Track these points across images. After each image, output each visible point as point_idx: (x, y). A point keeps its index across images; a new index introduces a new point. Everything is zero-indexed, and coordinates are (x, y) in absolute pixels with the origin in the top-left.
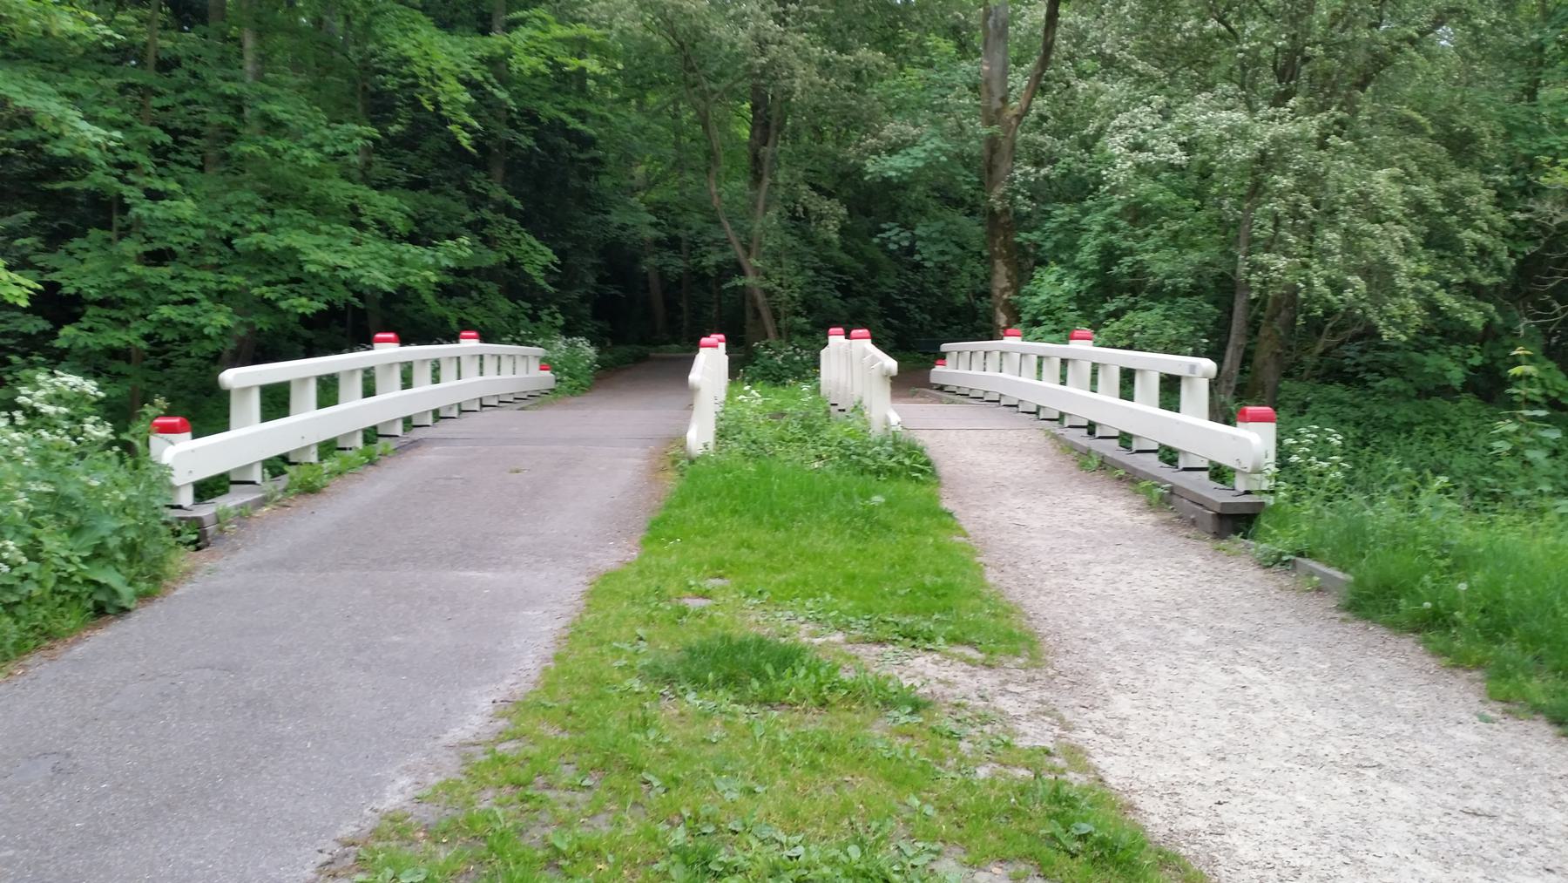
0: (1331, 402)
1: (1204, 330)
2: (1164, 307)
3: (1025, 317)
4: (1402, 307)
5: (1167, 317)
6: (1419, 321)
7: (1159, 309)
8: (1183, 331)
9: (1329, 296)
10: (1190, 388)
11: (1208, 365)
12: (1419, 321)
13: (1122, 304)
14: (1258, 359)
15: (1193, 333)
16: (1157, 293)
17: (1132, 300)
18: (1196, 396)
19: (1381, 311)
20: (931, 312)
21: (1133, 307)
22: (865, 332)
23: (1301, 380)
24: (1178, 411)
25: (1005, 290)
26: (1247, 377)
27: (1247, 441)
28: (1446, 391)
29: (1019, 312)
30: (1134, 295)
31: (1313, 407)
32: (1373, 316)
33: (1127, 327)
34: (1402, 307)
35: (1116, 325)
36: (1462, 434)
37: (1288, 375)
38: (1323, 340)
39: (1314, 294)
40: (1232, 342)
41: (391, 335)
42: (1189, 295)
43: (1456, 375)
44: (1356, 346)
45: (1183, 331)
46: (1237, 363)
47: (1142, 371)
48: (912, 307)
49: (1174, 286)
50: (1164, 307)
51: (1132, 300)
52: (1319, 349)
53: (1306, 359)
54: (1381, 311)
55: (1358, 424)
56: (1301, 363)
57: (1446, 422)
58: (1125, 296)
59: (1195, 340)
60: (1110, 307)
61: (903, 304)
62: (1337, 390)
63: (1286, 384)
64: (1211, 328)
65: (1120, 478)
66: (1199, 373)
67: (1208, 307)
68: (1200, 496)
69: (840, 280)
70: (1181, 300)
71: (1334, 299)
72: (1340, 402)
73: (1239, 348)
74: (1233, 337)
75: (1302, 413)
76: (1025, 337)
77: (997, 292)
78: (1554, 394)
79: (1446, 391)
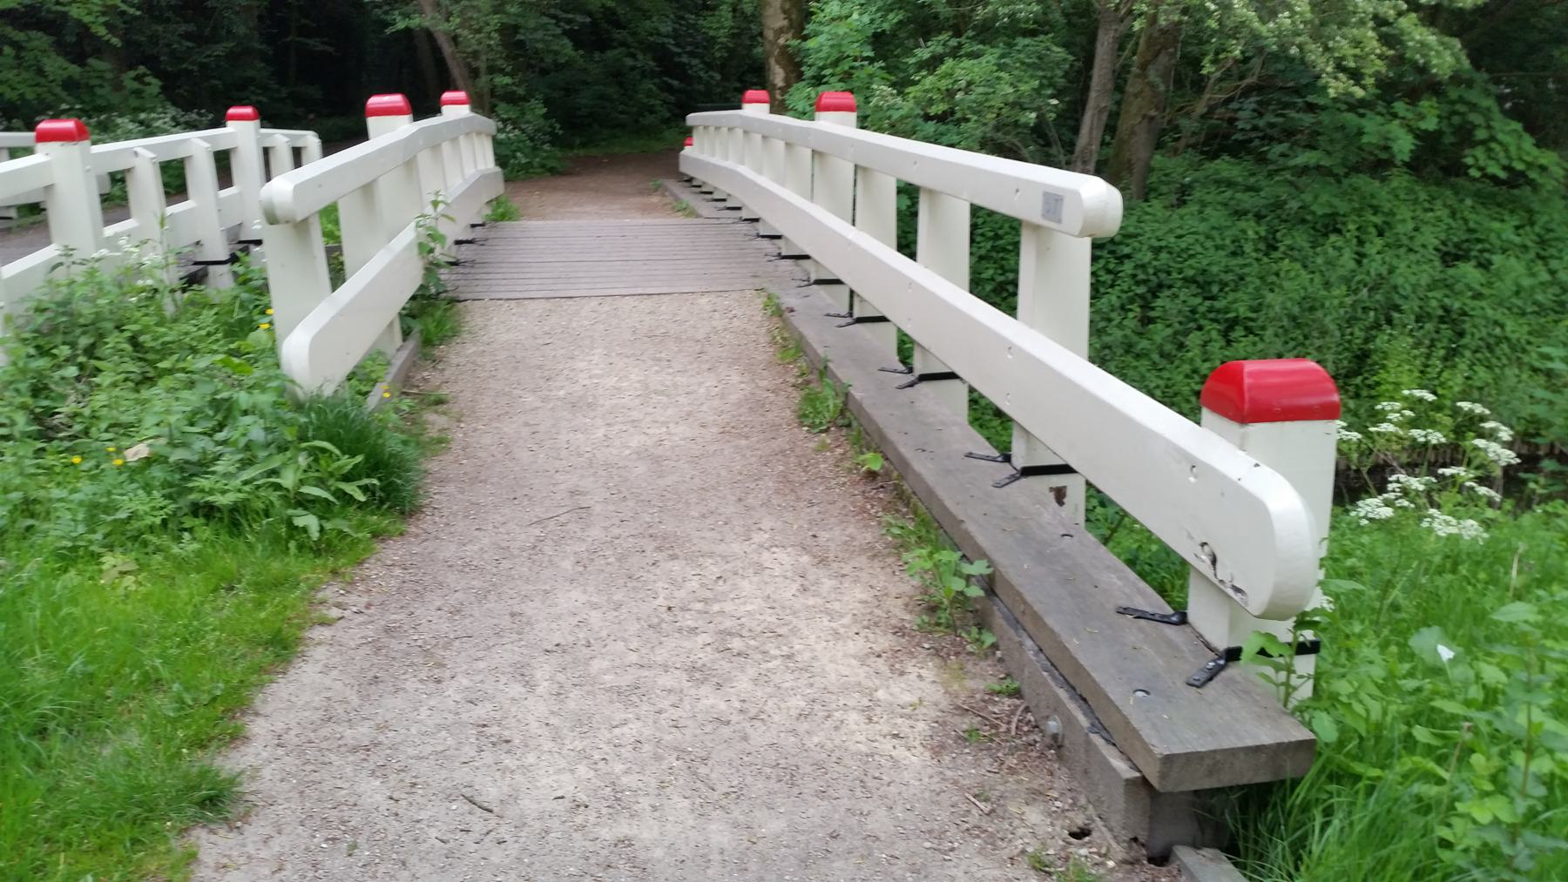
0: (1218, 182)
1: (1051, 85)
2: (997, 52)
3: (809, 73)
4: (1357, 43)
5: (1001, 67)
6: (1380, 66)
7: (991, 56)
8: (1023, 87)
9: (1256, 25)
10: (1042, 254)
11: (1095, 197)
12: (1380, 66)
13: (940, 50)
14: (1124, 125)
15: (1037, 91)
16: (987, 32)
17: (954, 42)
18: (1059, 277)
19: (1327, 49)
20: (722, 68)
21: (955, 53)
22: (396, 99)
23: (1176, 152)
24: (1011, 310)
25: (780, 31)
26: (1110, 151)
27: (1256, 508)
28: (1379, 165)
29: (800, 64)
30: (958, 34)
31: (1197, 194)
32: (1315, 54)
33: (944, 84)
34: (1357, 43)
35: (929, 81)
36: (1400, 229)
37: (1159, 146)
38: (1206, 96)
39: (1230, 23)
40: (1091, 103)
41: (248, 110)
42: (1032, 33)
43: (1404, 145)
44: (1251, 103)
45: (1023, 87)
46: (1098, 134)
47: (931, 192)
48: (695, 62)
49: (1012, 16)
50: (997, 52)
51: (954, 42)
52: (1201, 108)
53: (1184, 123)
54: (1327, 49)
55: (1259, 217)
56: (1176, 129)
57: (1376, 210)
58: (943, 37)
59: (1039, 102)
60: (923, 53)
61: (685, 59)
62: (1225, 167)
63: (1158, 159)
64: (1061, 82)
65: (872, 475)
66: (1072, 219)
67: (1059, 52)
68: (1079, 668)
69: (569, 21)
70: (1022, 42)
71: (1263, 30)
72: (1230, 184)
73: (1101, 111)
74: (1093, 95)
75: (1182, 203)
76: (779, 108)
77: (770, 34)
78: (1519, 166)
79: (1379, 165)
